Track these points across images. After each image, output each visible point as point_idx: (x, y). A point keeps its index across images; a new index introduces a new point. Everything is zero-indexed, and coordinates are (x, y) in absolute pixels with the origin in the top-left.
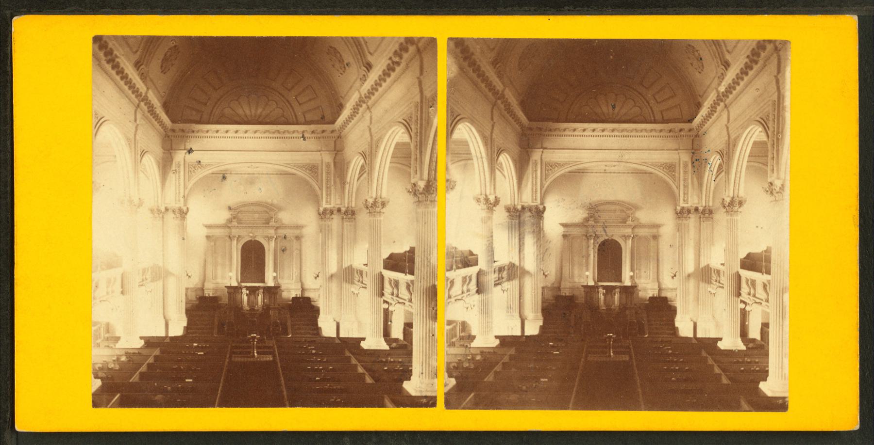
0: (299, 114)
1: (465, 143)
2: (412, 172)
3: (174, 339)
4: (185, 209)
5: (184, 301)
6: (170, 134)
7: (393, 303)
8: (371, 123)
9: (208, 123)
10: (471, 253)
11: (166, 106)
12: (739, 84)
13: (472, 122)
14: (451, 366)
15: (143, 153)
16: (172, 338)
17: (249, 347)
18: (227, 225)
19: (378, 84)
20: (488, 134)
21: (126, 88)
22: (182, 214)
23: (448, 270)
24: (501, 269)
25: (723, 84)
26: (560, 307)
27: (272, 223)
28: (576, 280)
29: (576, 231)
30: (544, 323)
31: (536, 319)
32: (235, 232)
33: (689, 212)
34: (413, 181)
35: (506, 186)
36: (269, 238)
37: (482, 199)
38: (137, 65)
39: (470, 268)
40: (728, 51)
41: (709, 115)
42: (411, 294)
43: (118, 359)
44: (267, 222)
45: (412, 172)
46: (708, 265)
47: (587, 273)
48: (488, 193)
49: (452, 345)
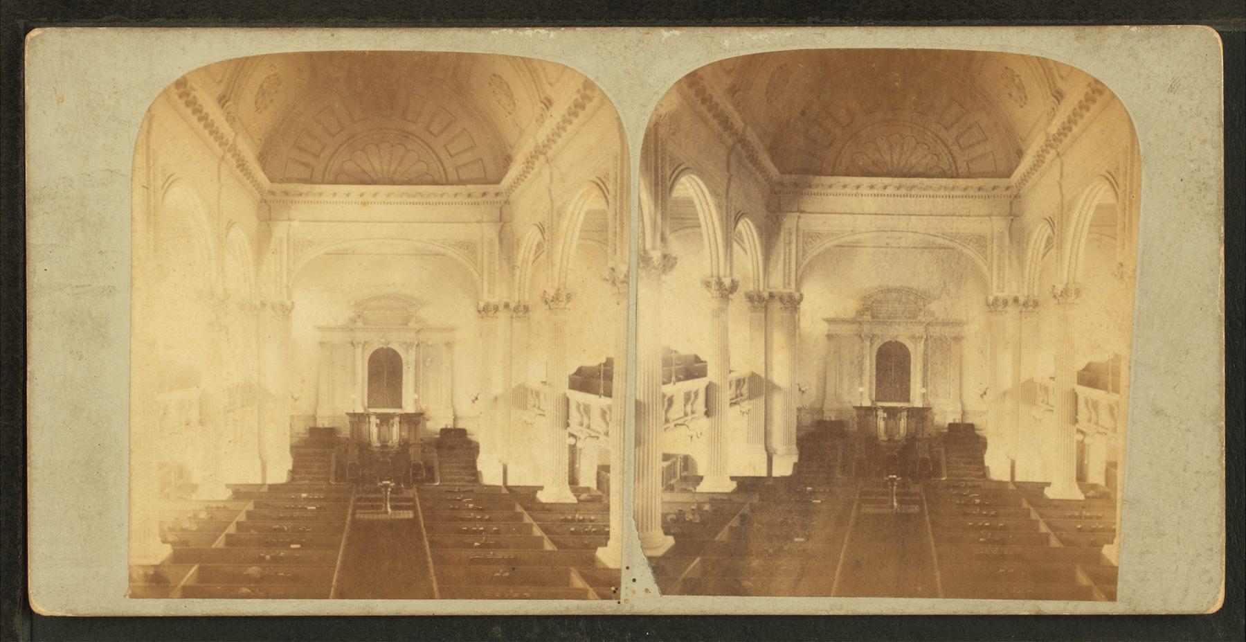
0: (451, 171)
1: (690, 203)
2: (610, 250)
3: (274, 488)
4: (289, 304)
5: (288, 433)
6: (269, 198)
7: (583, 437)
8: (552, 182)
9: (323, 183)
10: (697, 359)
11: (262, 158)
12: (1076, 124)
13: (701, 174)
14: (669, 518)
15: (230, 225)
16: (271, 487)
17: (380, 500)
18: (348, 328)
19: (561, 128)
20: (721, 191)
21: (206, 132)
22: (286, 311)
23: (664, 383)
24: (739, 383)
25: (1054, 122)
26: (821, 439)
27: (412, 324)
28: (846, 398)
29: (846, 330)
30: (800, 459)
31: (789, 453)
32: (360, 336)
33: (1005, 303)
34: (611, 264)
35: (747, 258)
36: (408, 346)
37: (713, 283)
38: (222, 100)
39: (696, 381)
40: (1062, 77)
41: (1035, 167)
42: (608, 424)
43: (195, 516)
44: (406, 322)
45: (610, 250)
46: (1031, 380)
47: (861, 389)
48: (722, 273)
49: (669, 488)
